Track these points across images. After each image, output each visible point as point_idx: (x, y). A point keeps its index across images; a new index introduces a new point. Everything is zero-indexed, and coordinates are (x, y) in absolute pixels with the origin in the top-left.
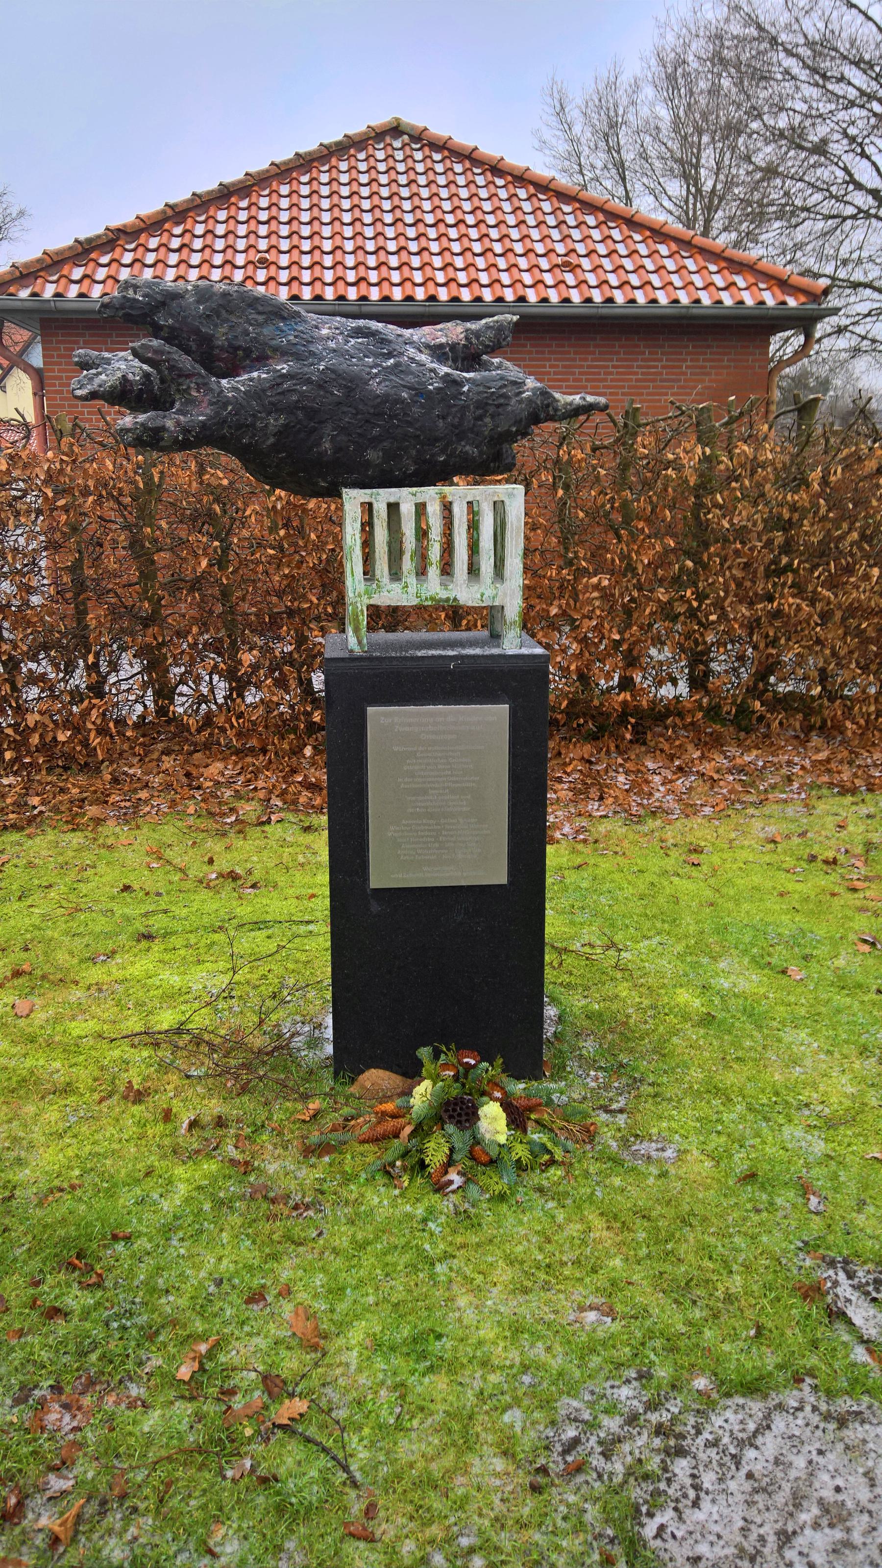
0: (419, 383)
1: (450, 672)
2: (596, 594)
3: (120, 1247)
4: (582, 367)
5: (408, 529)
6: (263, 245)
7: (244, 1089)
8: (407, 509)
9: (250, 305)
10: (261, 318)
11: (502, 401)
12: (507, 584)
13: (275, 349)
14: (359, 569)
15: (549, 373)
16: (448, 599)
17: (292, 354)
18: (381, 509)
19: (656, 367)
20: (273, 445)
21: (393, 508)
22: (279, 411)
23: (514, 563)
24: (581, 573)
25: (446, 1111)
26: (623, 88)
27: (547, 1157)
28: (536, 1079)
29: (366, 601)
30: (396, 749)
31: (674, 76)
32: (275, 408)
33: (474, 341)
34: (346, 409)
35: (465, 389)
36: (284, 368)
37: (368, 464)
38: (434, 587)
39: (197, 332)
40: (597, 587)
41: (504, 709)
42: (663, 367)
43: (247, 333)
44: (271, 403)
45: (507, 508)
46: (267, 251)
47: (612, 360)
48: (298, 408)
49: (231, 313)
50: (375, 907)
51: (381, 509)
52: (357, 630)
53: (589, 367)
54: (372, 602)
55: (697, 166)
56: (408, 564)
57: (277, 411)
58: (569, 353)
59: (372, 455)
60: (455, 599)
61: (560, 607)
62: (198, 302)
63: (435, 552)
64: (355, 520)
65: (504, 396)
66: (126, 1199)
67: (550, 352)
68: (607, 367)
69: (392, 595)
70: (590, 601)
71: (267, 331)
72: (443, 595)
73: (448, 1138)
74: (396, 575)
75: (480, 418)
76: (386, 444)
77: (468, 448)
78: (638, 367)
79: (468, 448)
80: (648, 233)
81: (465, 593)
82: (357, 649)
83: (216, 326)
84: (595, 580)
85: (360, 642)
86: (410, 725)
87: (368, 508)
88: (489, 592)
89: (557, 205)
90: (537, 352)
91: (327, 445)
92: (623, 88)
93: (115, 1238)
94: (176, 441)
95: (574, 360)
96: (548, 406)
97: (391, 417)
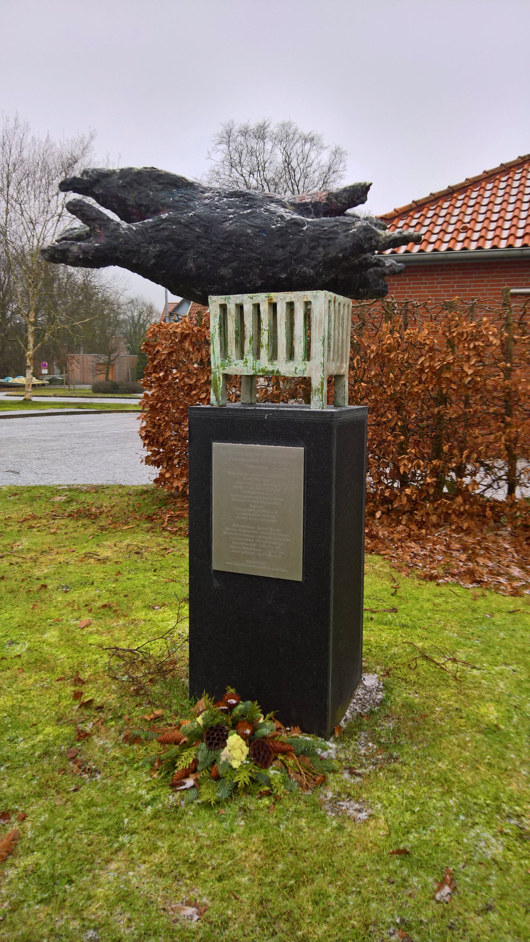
0: (265, 224)
6: (467, 219)
8: (248, 309)
9: (154, 180)
10: (160, 187)
11: (331, 236)
12: (312, 361)
13: (163, 205)
16: (273, 371)
17: (173, 207)
18: (232, 308)
20: (154, 264)
21: (240, 308)
22: (158, 242)
27: (267, 788)
28: (320, 735)
29: (222, 371)
30: (230, 473)
32: (153, 240)
33: (334, 200)
34: (204, 240)
35: (305, 228)
36: (164, 216)
37: (223, 278)
38: (264, 363)
39: (117, 197)
41: (300, 450)
43: (148, 196)
46: (469, 223)
49: (141, 184)
50: (216, 584)
51: (232, 308)
54: (225, 372)
57: (155, 242)
59: (224, 271)
60: (278, 372)
62: (120, 179)
63: (265, 338)
64: (215, 317)
65: (336, 233)
69: (239, 368)
71: (162, 194)
72: (270, 368)
74: (242, 355)
75: (314, 248)
76: (235, 264)
77: (305, 269)
83: (129, 192)
85: (217, 399)
87: (223, 308)
88: (301, 367)
94: (77, 258)
96: (371, 239)
97: (238, 246)
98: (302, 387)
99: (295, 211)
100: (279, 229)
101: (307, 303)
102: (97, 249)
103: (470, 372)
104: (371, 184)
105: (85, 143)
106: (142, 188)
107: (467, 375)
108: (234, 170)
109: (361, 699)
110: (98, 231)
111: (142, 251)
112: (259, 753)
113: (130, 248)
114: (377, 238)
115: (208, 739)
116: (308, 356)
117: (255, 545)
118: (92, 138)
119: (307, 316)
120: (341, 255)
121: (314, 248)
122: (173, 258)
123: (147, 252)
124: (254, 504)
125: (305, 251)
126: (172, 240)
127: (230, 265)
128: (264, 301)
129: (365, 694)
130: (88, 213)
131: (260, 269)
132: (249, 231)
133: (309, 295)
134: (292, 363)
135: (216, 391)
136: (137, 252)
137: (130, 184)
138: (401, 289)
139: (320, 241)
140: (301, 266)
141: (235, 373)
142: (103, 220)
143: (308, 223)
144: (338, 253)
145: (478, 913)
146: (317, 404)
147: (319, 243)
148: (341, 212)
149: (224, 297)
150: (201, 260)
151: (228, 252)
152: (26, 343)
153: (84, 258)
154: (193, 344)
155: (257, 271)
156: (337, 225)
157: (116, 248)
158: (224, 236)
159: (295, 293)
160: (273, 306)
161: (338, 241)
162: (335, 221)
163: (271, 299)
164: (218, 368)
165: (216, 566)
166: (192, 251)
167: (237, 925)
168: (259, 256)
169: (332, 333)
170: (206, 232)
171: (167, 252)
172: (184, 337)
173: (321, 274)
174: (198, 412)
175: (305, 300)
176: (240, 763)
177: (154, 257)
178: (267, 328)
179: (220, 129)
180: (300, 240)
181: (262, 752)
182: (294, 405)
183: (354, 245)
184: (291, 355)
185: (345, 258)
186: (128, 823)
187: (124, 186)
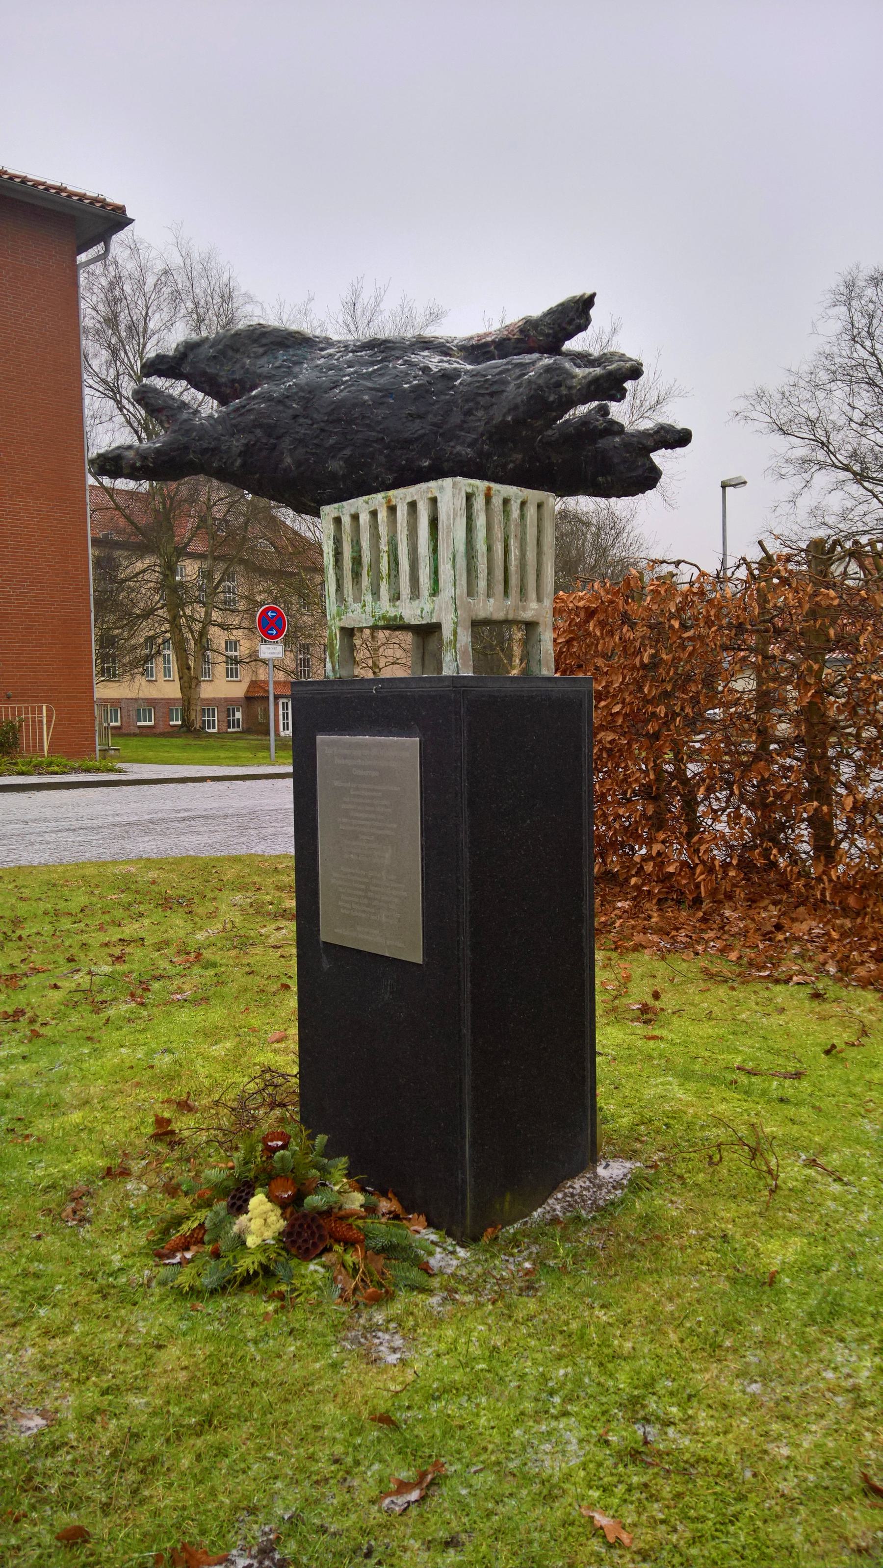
10: (261, 350)
11: (495, 388)
22: (242, 431)
37: (333, 476)
38: (385, 607)
48: (255, 426)
54: (343, 624)
59: (335, 465)
65: (505, 383)
72: (392, 612)
75: (469, 413)
76: (347, 452)
77: (458, 448)
79: (458, 448)
83: (222, 365)
88: (428, 607)
91: (288, 460)
94: (133, 467)
96: (558, 385)
97: (349, 422)
99: (465, 359)
100: (414, 389)
101: (434, 501)
102: (158, 451)
104: (593, 296)
105: (605, 341)
106: (238, 356)
108: (858, 346)
109: (572, 1195)
111: (223, 448)
112: (299, 1234)
113: (205, 445)
114: (568, 382)
117: (366, 901)
118: (614, 331)
119: (434, 522)
120: (509, 418)
121: (469, 413)
122: (264, 453)
123: (229, 448)
125: (456, 418)
126: (260, 426)
127: (340, 455)
129: (587, 1189)
130: (153, 401)
131: (386, 457)
132: (366, 397)
133: (432, 487)
135: (332, 656)
136: (215, 451)
137: (223, 353)
139: (480, 399)
140: (452, 444)
142: (171, 408)
143: (467, 372)
144: (505, 415)
145: (429, 1545)
147: (478, 403)
148: (554, 349)
149: (336, 505)
150: (301, 451)
151: (336, 433)
152: (510, 657)
153: (142, 467)
154: (602, 624)
155: (382, 459)
156: (508, 370)
157: (186, 448)
158: (329, 409)
159: (418, 486)
160: (392, 509)
161: (505, 394)
162: (507, 364)
163: (389, 501)
165: (323, 937)
166: (287, 439)
167: (69, 1457)
168: (380, 435)
169: (481, 546)
170: (305, 408)
171: (254, 445)
172: (591, 613)
173: (489, 455)
175: (430, 495)
176: (259, 1241)
177: (240, 455)
178: (386, 549)
179: (834, 282)
180: (448, 402)
181: (308, 1233)
183: (530, 398)
185: (518, 422)
186: (59, 1291)
187: (214, 357)
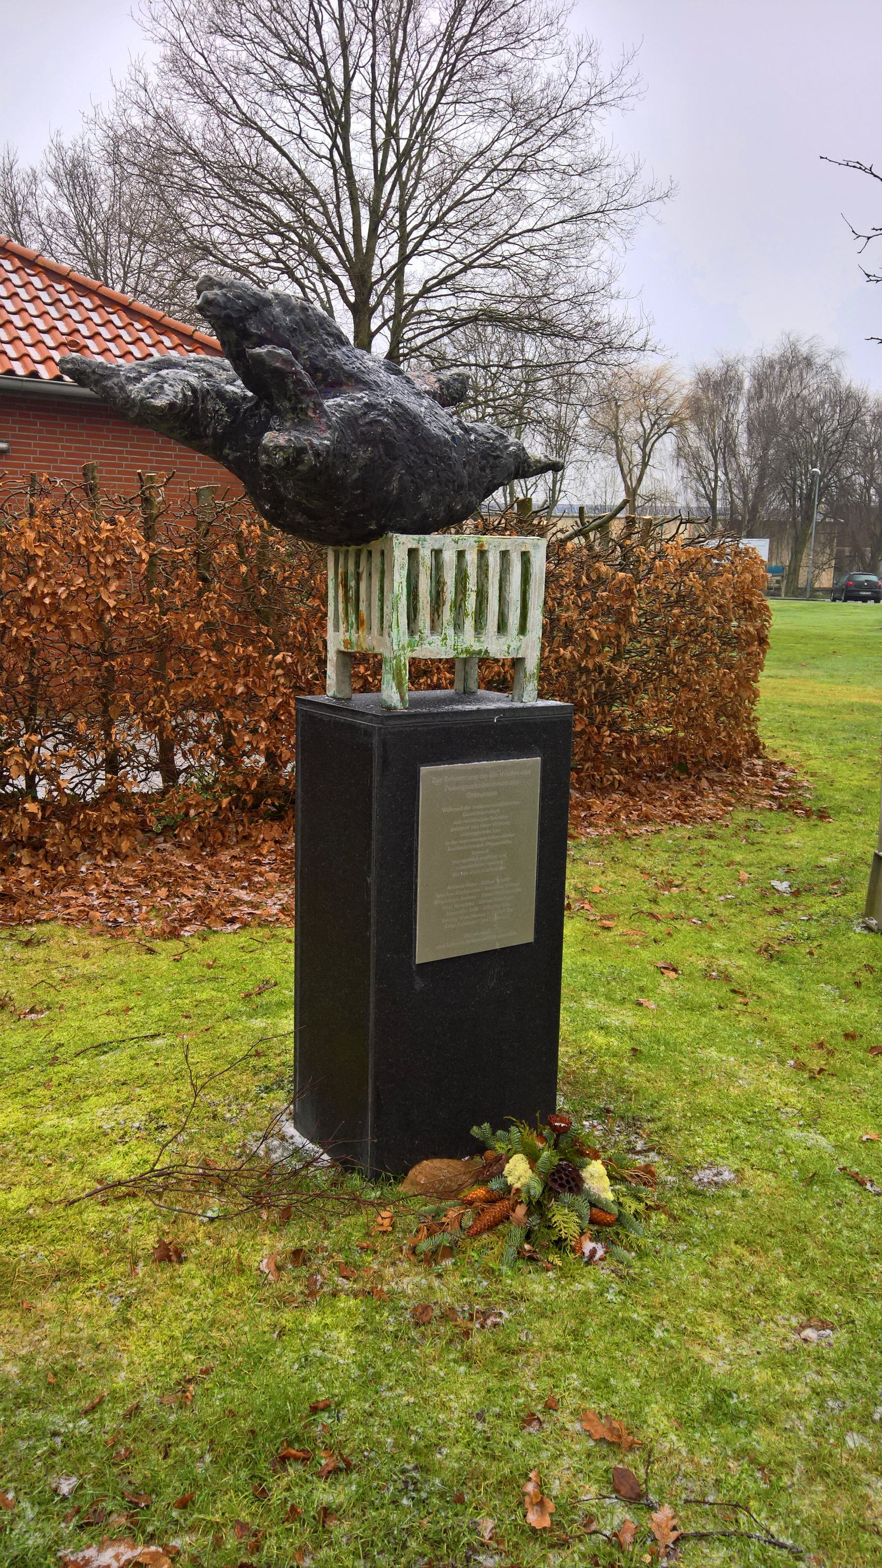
1: (494, 726)
2: (280, 672)
3: (324, 1418)
4: (96, 450)
5: (449, 577)
7: (287, 1215)
14: (404, 621)
15: (61, 454)
19: (170, 456)
23: (536, 617)
24: (266, 650)
25: (555, 1181)
26: (20, 176)
29: (409, 654)
30: (444, 810)
31: (74, 177)
38: (469, 640)
40: (280, 665)
42: (177, 456)
44: (362, 433)
45: (532, 559)
47: (125, 446)
52: (399, 686)
53: (103, 451)
54: (414, 655)
55: (106, 264)
56: (447, 614)
58: (81, 435)
61: (246, 686)
66: (286, 1361)
67: (62, 433)
68: (121, 452)
69: (435, 647)
70: (275, 677)
72: (476, 647)
73: (571, 1207)
78: (152, 454)
80: (148, 323)
81: (497, 647)
82: (399, 705)
84: (279, 657)
86: (457, 784)
88: (514, 645)
89: (49, 283)
90: (48, 432)
92: (20, 176)
93: (314, 1410)
95: (88, 443)
98: (503, 676)
103: (112, 603)
107: (108, 608)
110: (311, 414)
115: (562, 1186)
116: (523, 630)
124: (476, 849)
128: (472, 547)
134: (503, 639)
138: (108, 472)
141: (428, 655)
146: (529, 697)
149: (416, 537)
164: (404, 648)
174: (398, 722)
182: (495, 701)
184: (502, 627)
